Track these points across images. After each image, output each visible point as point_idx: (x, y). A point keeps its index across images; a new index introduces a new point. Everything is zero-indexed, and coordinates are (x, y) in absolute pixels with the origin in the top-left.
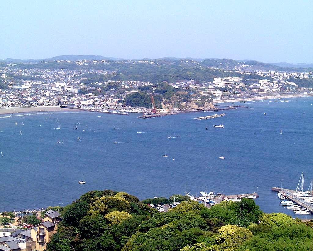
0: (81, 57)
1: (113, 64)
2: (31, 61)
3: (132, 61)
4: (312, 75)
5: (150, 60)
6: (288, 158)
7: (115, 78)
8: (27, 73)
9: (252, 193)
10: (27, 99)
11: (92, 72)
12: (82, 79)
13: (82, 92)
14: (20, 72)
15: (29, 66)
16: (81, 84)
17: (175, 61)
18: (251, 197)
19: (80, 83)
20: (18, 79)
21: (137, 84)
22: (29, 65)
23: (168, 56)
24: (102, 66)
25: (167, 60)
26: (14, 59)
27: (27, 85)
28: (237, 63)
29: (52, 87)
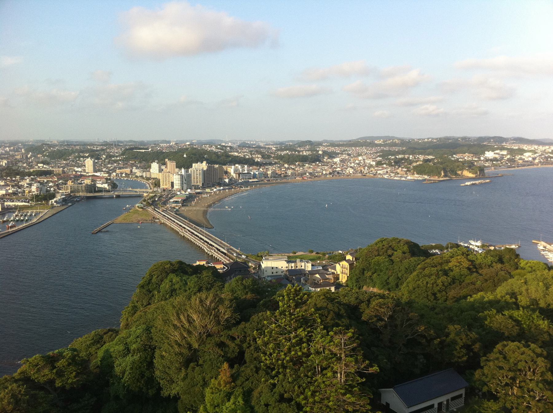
0: (379, 138)
1: (403, 142)
2: (341, 141)
3: (418, 139)
4: (551, 155)
5: (433, 139)
6: (258, 384)
7: (403, 153)
8: (337, 149)
9: (514, 244)
10: (337, 170)
11: (387, 149)
12: (379, 154)
13: (379, 164)
14: (331, 149)
15: (339, 146)
16: (378, 158)
17: (454, 139)
18: (513, 247)
19: (377, 158)
20: (332, 155)
21: (421, 157)
22: (366, 142)
23: (448, 136)
24: (395, 145)
25: (447, 138)
26: (391, 136)
27: (337, 160)
28: (506, 140)
29: (355, 160)
